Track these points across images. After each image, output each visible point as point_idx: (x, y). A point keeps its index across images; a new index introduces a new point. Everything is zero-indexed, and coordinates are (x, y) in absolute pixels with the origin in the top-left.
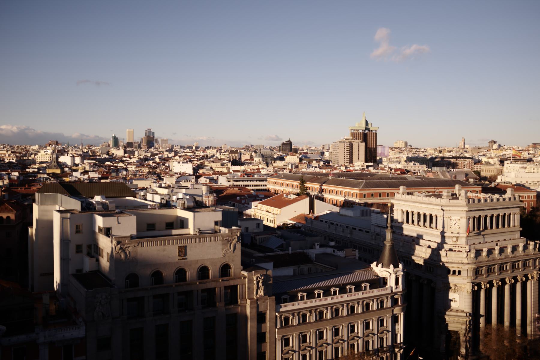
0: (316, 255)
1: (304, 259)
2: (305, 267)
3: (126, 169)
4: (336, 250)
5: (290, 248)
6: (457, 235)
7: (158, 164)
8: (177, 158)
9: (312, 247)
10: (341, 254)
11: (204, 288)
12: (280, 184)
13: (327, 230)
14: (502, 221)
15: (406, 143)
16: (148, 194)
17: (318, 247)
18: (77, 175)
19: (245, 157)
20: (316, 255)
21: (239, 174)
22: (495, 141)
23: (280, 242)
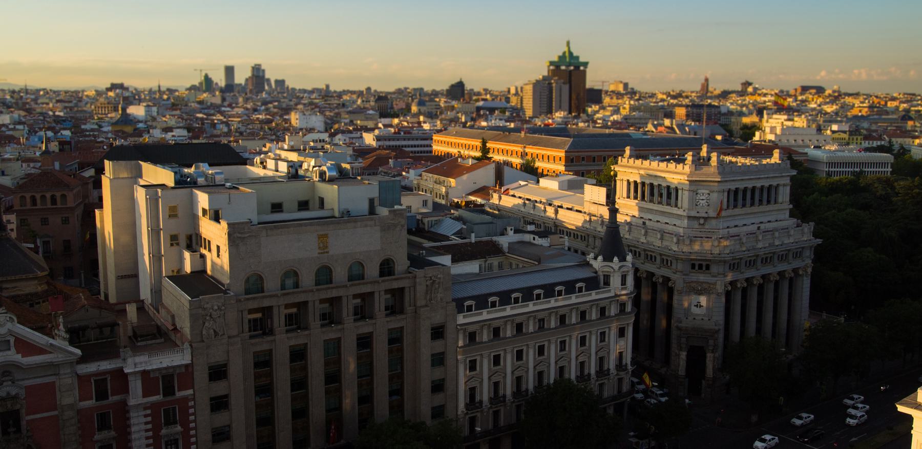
0: (509, 243)
1: (493, 249)
2: (495, 261)
3: (227, 124)
4: (537, 237)
5: (473, 235)
6: (706, 215)
7: (273, 115)
8: (300, 107)
9: (502, 234)
10: (539, 241)
11: (808, 305)
12: (451, 144)
13: (522, 209)
14: (766, 195)
15: (626, 85)
16: (268, 160)
17: (511, 233)
18: (157, 134)
19: (399, 105)
20: (509, 243)
21: (392, 130)
22: (750, 81)
23: (458, 226)
